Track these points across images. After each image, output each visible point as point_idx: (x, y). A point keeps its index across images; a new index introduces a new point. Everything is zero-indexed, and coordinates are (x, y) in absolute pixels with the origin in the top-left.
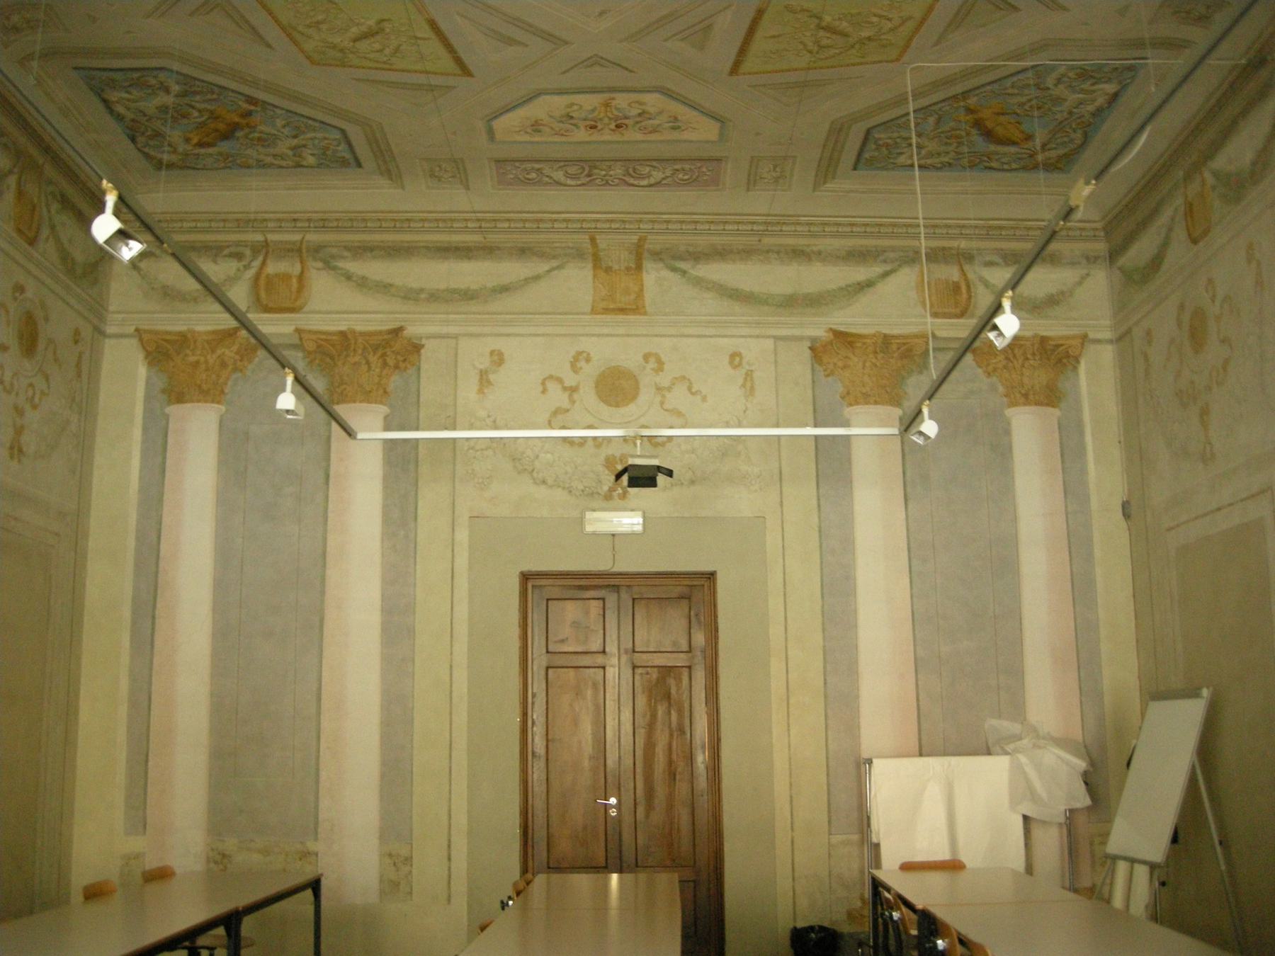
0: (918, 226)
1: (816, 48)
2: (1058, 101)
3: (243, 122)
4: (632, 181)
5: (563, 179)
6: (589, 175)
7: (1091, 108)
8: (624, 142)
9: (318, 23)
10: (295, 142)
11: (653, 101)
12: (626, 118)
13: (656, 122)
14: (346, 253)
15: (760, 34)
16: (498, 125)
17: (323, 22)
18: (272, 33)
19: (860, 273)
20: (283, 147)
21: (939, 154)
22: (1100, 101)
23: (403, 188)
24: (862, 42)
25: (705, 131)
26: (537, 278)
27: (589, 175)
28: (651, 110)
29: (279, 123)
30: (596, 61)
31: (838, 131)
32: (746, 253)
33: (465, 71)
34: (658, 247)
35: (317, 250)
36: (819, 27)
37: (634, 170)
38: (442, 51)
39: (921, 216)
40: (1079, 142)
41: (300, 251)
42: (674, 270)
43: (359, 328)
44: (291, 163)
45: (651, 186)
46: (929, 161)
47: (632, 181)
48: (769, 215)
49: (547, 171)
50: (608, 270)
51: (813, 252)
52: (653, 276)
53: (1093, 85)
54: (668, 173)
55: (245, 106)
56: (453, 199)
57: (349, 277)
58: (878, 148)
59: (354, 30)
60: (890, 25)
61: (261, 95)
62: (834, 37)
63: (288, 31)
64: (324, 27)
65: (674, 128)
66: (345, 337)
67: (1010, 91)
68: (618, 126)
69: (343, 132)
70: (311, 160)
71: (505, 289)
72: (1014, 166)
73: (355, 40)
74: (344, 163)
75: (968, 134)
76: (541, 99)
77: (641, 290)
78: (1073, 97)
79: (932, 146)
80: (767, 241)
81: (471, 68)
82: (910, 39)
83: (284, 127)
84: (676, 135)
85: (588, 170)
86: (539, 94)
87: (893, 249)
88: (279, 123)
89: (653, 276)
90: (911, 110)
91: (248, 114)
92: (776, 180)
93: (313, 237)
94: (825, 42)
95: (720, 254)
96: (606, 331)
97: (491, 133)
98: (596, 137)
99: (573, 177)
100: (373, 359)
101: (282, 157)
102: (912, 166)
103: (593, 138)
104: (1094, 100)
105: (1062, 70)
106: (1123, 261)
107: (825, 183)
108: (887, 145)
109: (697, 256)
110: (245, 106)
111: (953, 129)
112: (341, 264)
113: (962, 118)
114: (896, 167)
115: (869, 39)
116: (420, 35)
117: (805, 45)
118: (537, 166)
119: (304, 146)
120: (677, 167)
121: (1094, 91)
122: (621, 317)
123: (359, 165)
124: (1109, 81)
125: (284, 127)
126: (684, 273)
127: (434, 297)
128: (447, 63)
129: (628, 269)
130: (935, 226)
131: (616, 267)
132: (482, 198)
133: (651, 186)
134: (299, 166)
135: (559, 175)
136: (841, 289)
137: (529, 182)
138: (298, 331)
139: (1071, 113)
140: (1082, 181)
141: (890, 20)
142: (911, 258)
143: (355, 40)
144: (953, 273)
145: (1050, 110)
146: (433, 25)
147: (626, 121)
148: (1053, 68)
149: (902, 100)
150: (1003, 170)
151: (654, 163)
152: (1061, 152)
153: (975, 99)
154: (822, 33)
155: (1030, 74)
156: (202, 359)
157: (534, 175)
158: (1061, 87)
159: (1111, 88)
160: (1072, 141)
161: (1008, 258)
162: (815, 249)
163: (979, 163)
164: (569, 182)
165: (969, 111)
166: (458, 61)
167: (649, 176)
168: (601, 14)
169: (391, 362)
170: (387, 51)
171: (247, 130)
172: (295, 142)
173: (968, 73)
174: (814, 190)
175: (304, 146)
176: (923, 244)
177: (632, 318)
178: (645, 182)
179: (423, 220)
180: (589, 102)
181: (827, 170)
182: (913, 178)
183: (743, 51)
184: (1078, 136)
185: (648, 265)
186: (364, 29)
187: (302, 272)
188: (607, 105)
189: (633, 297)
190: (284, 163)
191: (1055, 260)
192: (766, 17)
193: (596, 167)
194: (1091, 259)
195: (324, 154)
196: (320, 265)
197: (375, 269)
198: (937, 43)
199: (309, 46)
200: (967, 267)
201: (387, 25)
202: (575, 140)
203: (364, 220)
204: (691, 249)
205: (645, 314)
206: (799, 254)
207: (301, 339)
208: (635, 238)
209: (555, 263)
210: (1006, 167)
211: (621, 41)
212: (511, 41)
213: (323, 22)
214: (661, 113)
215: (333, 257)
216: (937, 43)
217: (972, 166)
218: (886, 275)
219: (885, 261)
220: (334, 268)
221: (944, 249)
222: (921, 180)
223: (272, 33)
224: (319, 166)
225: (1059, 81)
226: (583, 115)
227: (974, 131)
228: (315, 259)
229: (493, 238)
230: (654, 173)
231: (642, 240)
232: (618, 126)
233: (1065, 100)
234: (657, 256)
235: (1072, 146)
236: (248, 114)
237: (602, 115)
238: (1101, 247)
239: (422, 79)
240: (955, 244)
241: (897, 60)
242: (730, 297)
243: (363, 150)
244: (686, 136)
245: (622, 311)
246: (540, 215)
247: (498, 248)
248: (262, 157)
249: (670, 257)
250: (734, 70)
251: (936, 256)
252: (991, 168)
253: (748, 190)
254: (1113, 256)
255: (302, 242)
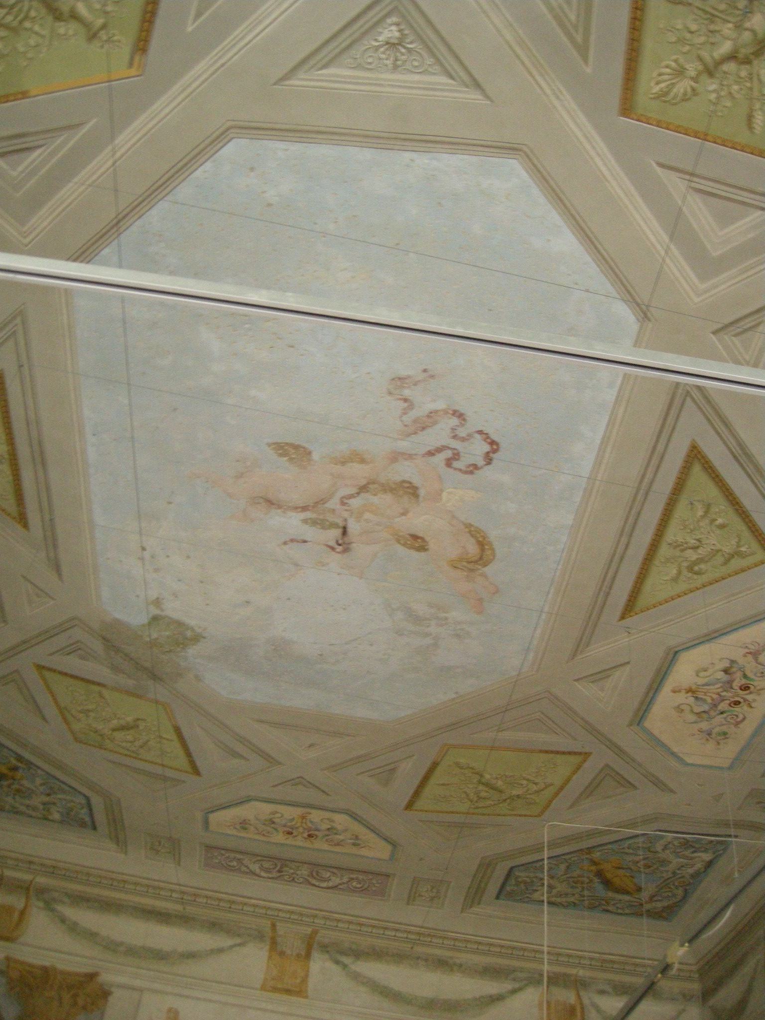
0: (543, 952)
1: (475, 799)
2: (664, 862)
3: (10, 774)
4: (314, 882)
5: (258, 871)
6: (279, 871)
7: (691, 871)
8: (314, 850)
9: (89, 711)
10: (47, 799)
11: (341, 820)
12: (318, 830)
13: (341, 837)
14: (66, 900)
15: (433, 780)
16: (212, 817)
17: (91, 711)
18: (51, 711)
19: (492, 987)
20: (36, 801)
21: (567, 894)
22: (699, 866)
23: (126, 853)
24: (512, 798)
25: (381, 851)
26: (221, 951)
27: (279, 871)
28: (340, 827)
29: (38, 781)
30: (299, 781)
31: (487, 865)
32: (399, 957)
33: (196, 772)
34: (326, 941)
35: (41, 891)
36: (480, 782)
37: (317, 873)
38: (181, 753)
39: (545, 943)
40: (679, 898)
41: (28, 889)
42: (337, 962)
43: (60, 966)
44: (40, 816)
45: (328, 888)
46: (559, 900)
47: (314, 882)
48: (422, 927)
49: (246, 862)
50: (282, 954)
51: (455, 964)
52: (319, 965)
53: (693, 852)
54: (345, 880)
55: (14, 761)
56: (165, 871)
57: (63, 920)
58: (518, 884)
59: (115, 722)
60: (535, 788)
61: (27, 755)
62: (491, 791)
63: (62, 711)
64: (92, 714)
65: (354, 844)
66: (47, 973)
67: (627, 851)
68: (310, 836)
69: (88, 799)
70: (57, 816)
71: (191, 956)
72: (627, 911)
73: (114, 730)
74: (83, 824)
75: (591, 881)
76: (253, 803)
77: (307, 976)
78: (676, 861)
79: (560, 887)
80: (420, 950)
81: (201, 770)
82: (551, 801)
83: (41, 785)
84: (354, 850)
85: (280, 867)
86: (250, 800)
87: (522, 970)
88: (38, 781)
89: (319, 965)
90: (546, 856)
91: (15, 769)
92: (432, 899)
93: (41, 880)
94: (483, 794)
95: (377, 954)
96: (270, 1007)
97: (206, 823)
98: (290, 841)
99: (268, 870)
100: (66, 997)
101: (35, 809)
102: (543, 901)
103: (288, 842)
104: (693, 866)
105: (669, 839)
106: (712, 1002)
107: (471, 907)
108: (525, 883)
109: (358, 954)
110: (14, 761)
111: (579, 876)
112: (59, 908)
113: (585, 868)
114: (531, 901)
115: (518, 796)
116: (164, 736)
117: (467, 795)
118: (239, 856)
119: (54, 804)
120: (352, 876)
121: (692, 859)
122: (285, 997)
123: (94, 828)
124: (706, 851)
125: (41, 785)
126: (345, 966)
127: (132, 952)
128: (182, 761)
129: (298, 956)
130: (559, 954)
131: (289, 952)
132: (187, 875)
133: (328, 888)
134: (46, 819)
135: (255, 867)
136: (475, 999)
137: (230, 869)
138: (8, 959)
139: (674, 873)
140: (677, 943)
141: (536, 784)
142: (534, 980)
143: (114, 730)
144: (569, 996)
145: (657, 869)
146: (178, 731)
147: (316, 833)
148: (662, 837)
149: (539, 849)
150: (618, 914)
151: (335, 870)
152: (665, 903)
153: (598, 854)
154: (481, 787)
155: (641, 840)
156: (642, 863)
157: (235, 863)
158: (668, 852)
159: (707, 857)
160: (674, 895)
161: (620, 989)
162: (458, 961)
163: (597, 906)
164: (263, 874)
165: (594, 863)
166: (193, 764)
167: (329, 880)
168: (311, 746)
169: (81, 1001)
170: (137, 743)
171: (11, 781)
172: (47, 799)
173: (591, 834)
174: (462, 912)
175: (54, 804)
176: (546, 967)
177: (294, 999)
178: (324, 885)
179: (136, 884)
180: (289, 813)
181: (474, 896)
182: (543, 912)
183: (417, 793)
184: (680, 892)
185: (315, 955)
186: (122, 722)
187: (25, 908)
188: (303, 817)
189: (298, 981)
190: (34, 814)
191: (658, 996)
192: (439, 768)
193: (286, 866)
194: (687, 997)
195: (68, 814)
196: (41, 904)
197: (87, 918)
198: (571, 807)
199: (76, 726)
200: (582, 993)
201: (142, 725)
202: (273, 841)
203: (88, 874)
204: (354, 947)
205: (306, 997)
206: (442, 964)
207: (8, 966)
208: (309, 930)
209: (238, 940)
210: (620, 911)
211: (322, 770)
212: (235, 754)
213: (91, 711)
214: (346, 830)
215: (54, 900)
216: (571, 807)
217: (592, 908)
218: (514, 992)
219: (514, 980)
220: (53, 910)
221: (565, 974)
222: (549, 913)
223: (51, 711)
224: (62, 822)
225: (665, 848)
226: (283, 822)
227: (596, 880)
228: (38, 900)
229: (190, 910)
230: (333, 878)
231: (315, 932)
232: (310, 836)
233: (671, 862)
234: (325, 948)
235: (675, 900)
236: (15, 769)
237: (299, 824)
238: (696, 987)
239: (159, 770)
240: (574, 971)
241: (539, 816)
242: (381, 993)
243: (100, 817)
244: (364, 852)
245: (288, 991)
246: (234, 898)
247: (193, 919)
248: (17, 805)
249: (337, 952)
250: (409, 806)
251: (555, 980)
252: (607, 911)
253: (408, 904)
254: (706, 995)
255: (31, 882)
